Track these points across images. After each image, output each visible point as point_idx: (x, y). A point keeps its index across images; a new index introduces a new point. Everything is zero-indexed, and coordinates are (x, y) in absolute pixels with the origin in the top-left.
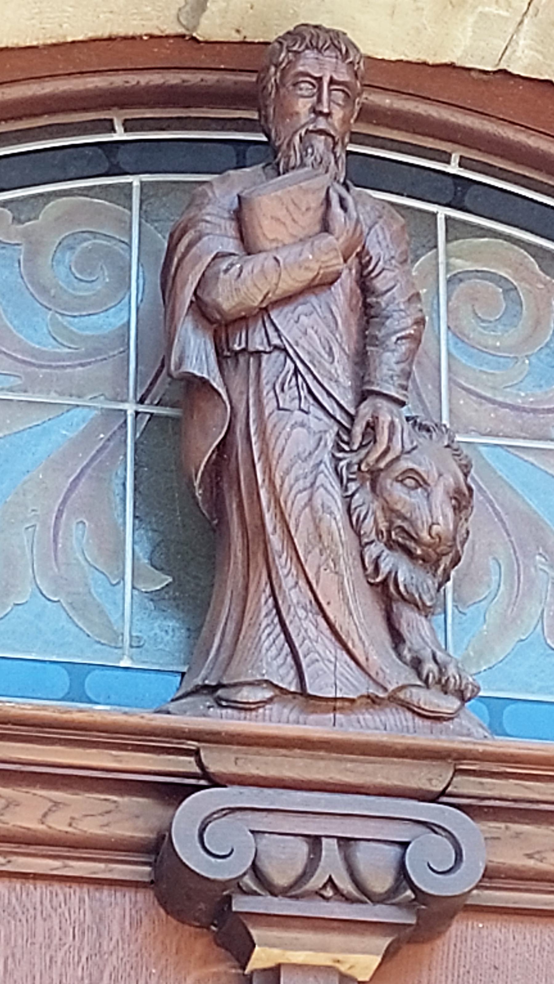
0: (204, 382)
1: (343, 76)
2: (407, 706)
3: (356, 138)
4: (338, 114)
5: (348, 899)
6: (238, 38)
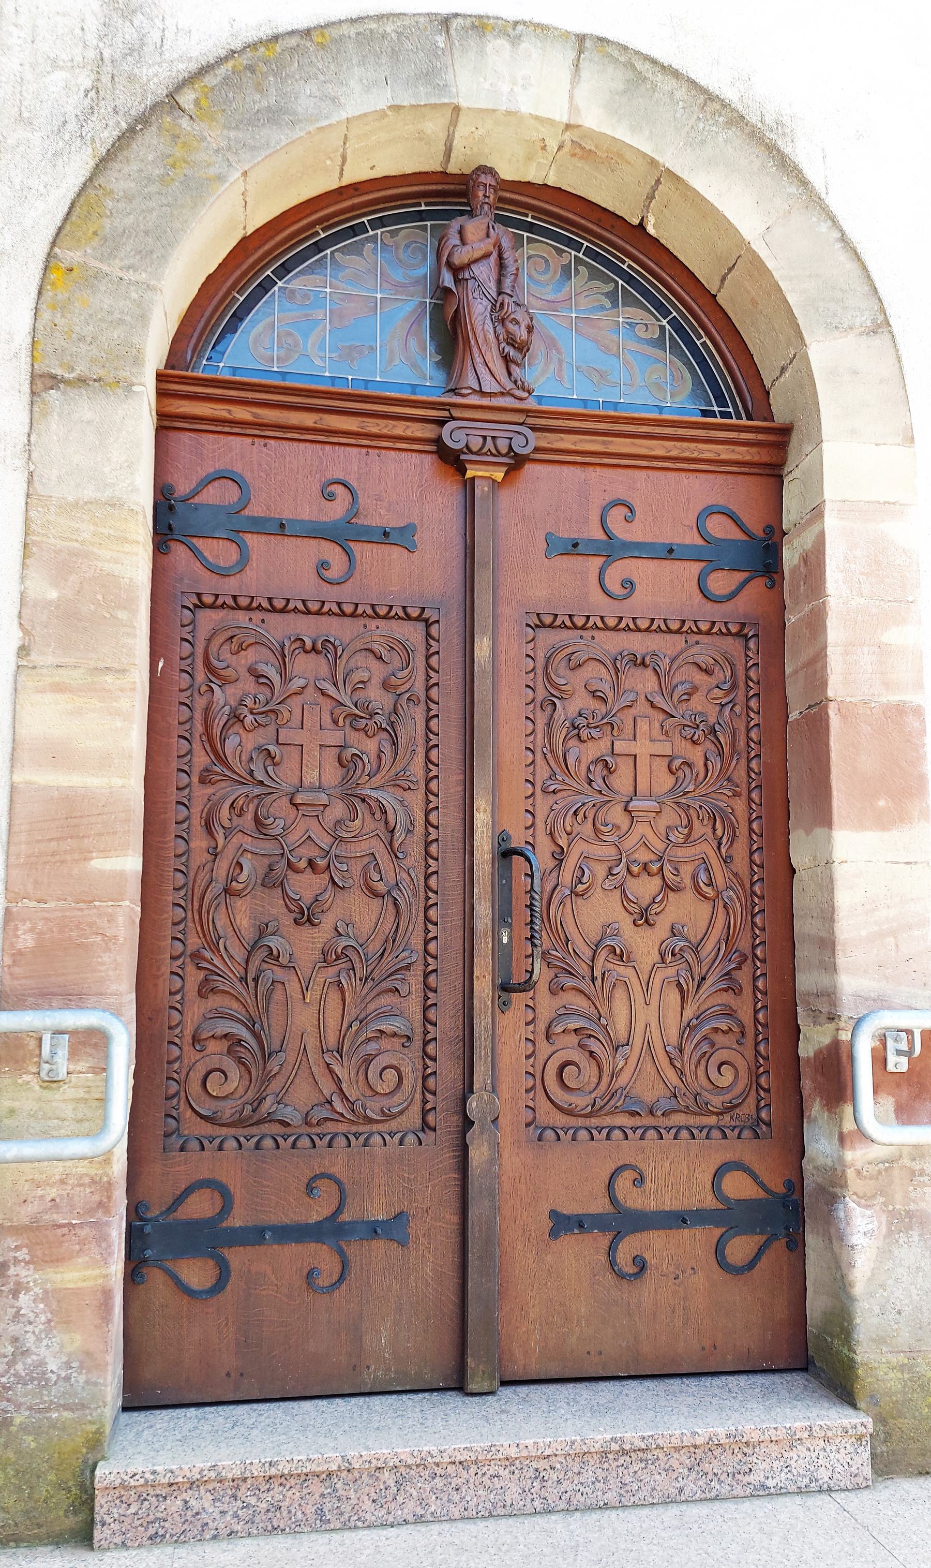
0: (451, 290)
1: (493, 183)
2: (513, 396)
3: (498, 208)
4: (492, 197)
5: (494, 455)
6: (460, 172)
